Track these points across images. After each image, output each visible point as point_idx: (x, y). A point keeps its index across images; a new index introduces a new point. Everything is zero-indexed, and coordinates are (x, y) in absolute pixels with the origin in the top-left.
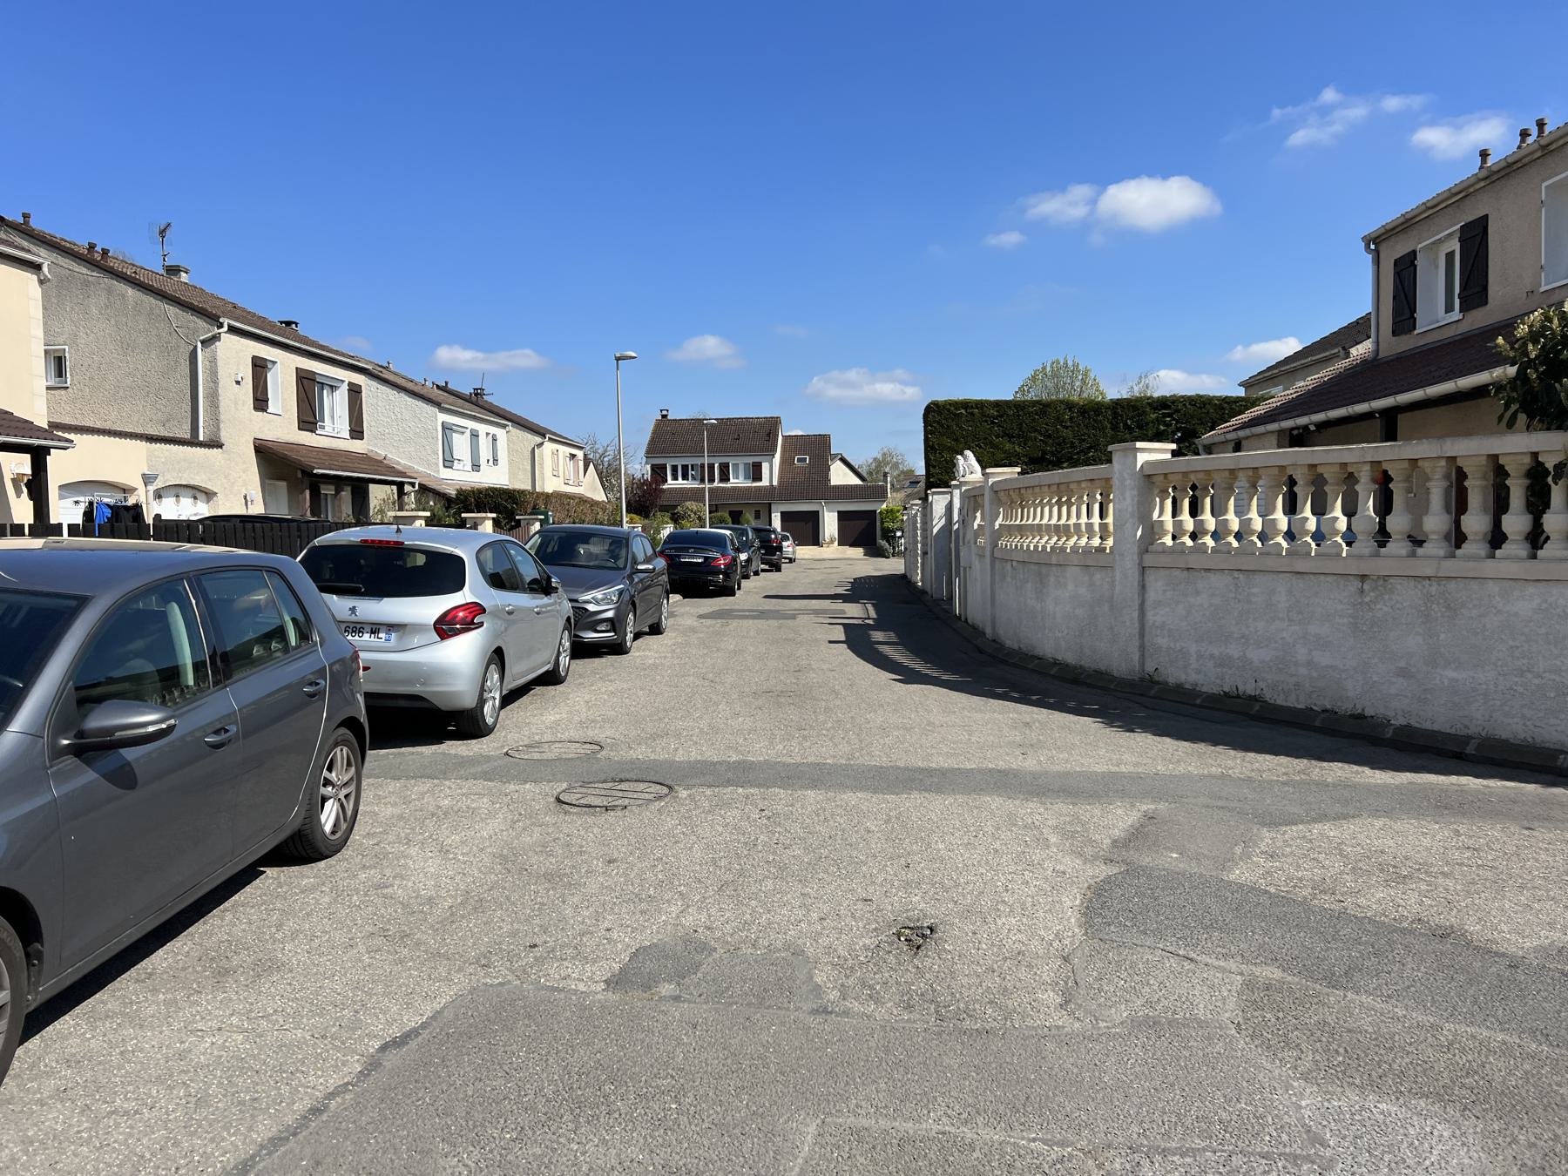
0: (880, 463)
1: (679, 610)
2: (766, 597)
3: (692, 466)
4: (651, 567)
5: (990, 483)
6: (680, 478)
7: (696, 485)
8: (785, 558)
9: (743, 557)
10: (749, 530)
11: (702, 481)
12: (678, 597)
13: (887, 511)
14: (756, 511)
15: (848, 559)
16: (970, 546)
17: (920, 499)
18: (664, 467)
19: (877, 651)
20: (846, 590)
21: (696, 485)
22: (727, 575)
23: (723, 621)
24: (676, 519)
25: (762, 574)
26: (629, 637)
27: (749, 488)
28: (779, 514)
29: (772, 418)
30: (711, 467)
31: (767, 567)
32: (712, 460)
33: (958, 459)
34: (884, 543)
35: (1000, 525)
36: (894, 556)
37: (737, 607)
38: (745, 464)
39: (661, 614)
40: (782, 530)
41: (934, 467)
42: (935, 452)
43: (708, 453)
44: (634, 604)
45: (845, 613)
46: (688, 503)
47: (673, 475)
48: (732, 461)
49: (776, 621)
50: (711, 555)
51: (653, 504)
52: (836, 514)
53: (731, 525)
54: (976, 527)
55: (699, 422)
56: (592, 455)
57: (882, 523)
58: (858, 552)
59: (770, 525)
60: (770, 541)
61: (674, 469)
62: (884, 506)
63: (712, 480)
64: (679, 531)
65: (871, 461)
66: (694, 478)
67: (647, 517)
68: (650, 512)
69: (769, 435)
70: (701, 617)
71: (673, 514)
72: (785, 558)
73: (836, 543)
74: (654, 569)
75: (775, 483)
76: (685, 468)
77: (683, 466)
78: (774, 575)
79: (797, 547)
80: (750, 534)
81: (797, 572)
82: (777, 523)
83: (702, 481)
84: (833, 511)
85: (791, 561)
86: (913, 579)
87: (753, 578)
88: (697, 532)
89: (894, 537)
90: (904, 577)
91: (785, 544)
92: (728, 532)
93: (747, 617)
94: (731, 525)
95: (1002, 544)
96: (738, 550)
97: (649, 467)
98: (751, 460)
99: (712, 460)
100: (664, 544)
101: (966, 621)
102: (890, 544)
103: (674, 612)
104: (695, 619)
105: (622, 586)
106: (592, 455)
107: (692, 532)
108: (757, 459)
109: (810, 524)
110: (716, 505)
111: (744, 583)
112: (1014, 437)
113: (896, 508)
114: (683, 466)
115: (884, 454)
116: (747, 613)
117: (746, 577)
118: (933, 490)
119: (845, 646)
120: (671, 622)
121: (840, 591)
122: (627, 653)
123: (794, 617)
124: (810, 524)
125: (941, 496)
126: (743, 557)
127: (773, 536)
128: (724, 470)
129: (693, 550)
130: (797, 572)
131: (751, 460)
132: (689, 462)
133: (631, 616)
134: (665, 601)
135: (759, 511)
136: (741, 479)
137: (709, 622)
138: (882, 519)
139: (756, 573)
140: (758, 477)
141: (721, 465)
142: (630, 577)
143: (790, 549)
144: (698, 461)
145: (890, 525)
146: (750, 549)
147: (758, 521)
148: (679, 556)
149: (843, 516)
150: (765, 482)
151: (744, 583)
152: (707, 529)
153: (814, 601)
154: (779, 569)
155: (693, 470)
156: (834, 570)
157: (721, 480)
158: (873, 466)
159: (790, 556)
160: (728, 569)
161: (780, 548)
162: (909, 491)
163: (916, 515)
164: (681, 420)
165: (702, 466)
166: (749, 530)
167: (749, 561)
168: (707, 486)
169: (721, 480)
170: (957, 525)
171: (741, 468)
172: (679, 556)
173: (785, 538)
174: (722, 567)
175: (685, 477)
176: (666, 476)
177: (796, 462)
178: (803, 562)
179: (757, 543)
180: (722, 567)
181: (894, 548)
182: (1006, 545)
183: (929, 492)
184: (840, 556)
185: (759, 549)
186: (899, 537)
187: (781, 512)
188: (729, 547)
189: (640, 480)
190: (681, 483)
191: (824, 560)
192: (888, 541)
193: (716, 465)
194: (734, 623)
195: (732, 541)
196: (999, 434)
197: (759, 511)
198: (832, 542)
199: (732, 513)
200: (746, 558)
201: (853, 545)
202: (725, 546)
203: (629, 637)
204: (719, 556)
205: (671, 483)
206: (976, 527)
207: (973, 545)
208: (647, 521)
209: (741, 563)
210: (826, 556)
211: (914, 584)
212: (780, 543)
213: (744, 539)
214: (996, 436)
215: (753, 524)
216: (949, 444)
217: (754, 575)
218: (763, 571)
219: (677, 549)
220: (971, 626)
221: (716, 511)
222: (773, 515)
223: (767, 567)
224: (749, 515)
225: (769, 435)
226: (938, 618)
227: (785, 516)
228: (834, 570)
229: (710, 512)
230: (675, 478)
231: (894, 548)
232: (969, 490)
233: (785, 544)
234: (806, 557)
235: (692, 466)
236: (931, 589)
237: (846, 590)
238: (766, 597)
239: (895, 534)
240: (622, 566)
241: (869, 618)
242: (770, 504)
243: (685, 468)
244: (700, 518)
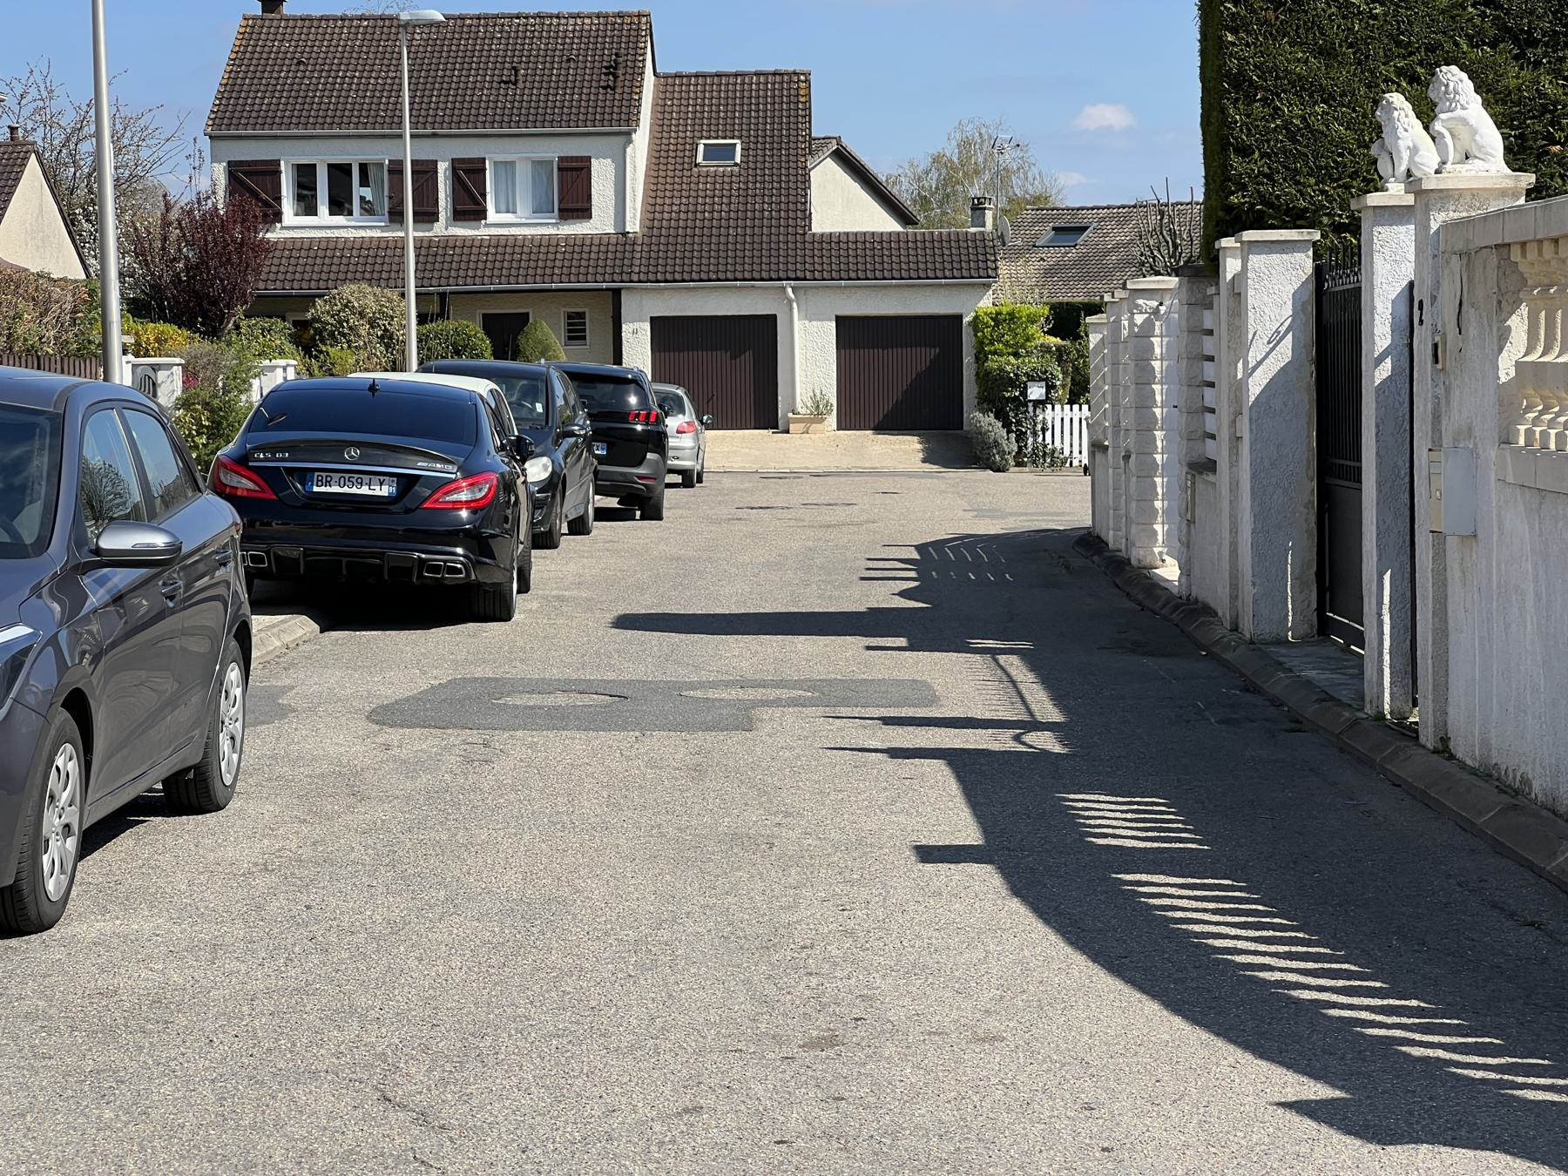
0: (951, 174)
1: (306, 684)
2: (626, 622)
3: (363, 168)
4: (159, 540)
5: (1434, 226)
6: (323, 208)
7: (371, 230)
8: (671, 471)
9: (537, 470)
10: (555, 376)
11: (396, 216)
12: (301, 626)
13: (997, 319)
14: (570, 316)
15: (875, 473)
16: (1473, 453)
17: (1176, 272)
18: (270, 171)
19: (1131, 900)
20: (903, 594)
21: (371, 230)
22: (480, 544)
23: (474, 736)
24: (308, 340)
25: (600, 529)
26: (59, 848)
27: (549, 244)
28: (647, 326)
29: (620, 15)
30: (425, 172)
31: (612, 502)
32: (427, 151)
33: (1391, 108)
34: (988, 423)
35: (1518, 364)
36: (1019, 464)
37: (518, 671)
38: (539, 164)
39: (216, 725)
40: (658, 376)
41: (1244, 152)
42: (1251, 100)
43: (414, 125)
44: (78, 704)
45: (934, 700)
46: (348, 290)
47: (300, 198)
48: (492, 153)
49: (674, 738)
50: (421, 468)
51: (234, 294)
52: (832, 326)
53: (489, 361)
54: (1506, 369)
55: (388, 25)
56: (40, 132)
57: (981, 357)
58: (905, 450)
59: (618, 359)
60: (624, 416)
61: (306, 176)
62: (986, 303)
63: (426, 215)
64: (322, 380)
65: (925, 163)
66: (368, 209)
67: (213, 331)
68: (222, 319)
69: (612, 70)
70: (386, 715)
71: (302, 325)
72: (671, 471)
73: (832, 420)
74: (174, 549)
75: (634, 225)
76: (340, 173)
77: (332, 168)
78: (635, 531)
79: (710, 433)
80: (559, 389)
81: (718, 521)
82: (638, 353)
83: (396, 216)
84: (821, 318)
85: (689, 479)
86: (1136, 555)
87: (568, 543)
88: (373, 387)
89: (1021, 403)
90: (1088, 541)
91: (672, 423)
92: (482, 387)
93: (557, 719)
94: (489, 361)
95: (1529, 433)
96: (520, 451)
97: (220, 172)
98: (554, 150)
99: (427, 151)
100: (249, 429)
101: (1444, 749)
102: (1007, 425)
103: (284, 690)
104: (363, 726)
105: (21, 631)
106: (40, 132)
107: (354, 388)
108: (574, 148)
109: (748, 356)
110: (442, 295)
111: (542, 562)
112: (1534, 43)
113: (1026, 310)
114: (332, 168)
115: (966, 144)
116: (561, 699)
117: (545, 540)
118: (1250, 235)
119: (985, 879)
120: (260, 742)
121: (885, 596)
122: (42, 925)
123: (741, 718)
124: (748, 356)
125: (1276, 258)
126: (537, 470)
127: (633, 400)
128: (469, 177)
129: (355, 452)
130: (718, 521)
131: (554, 150)
132: (352, 153)
133: (66, 761)
134: (234, 674)
135: (581, 315)
136: (523, 212)
137: (414, 742)
138: (981, 343)
139: (579, 527)
140: (575, 204)
141: (457, 166)
142: (67, 585)
143: (687, 441)
144: (379, 153)
145: (1010, 364)
146: (557, 443)
147: (576, 347)
148: (304, 475)
149: (852, 332)
150: (600, 223)
151: (542, 562)
152: (412, 376)
153: (803, 645)
154: (652, 512)
155: (364, 182)
156: (841, 514)
157: (459, 215)
158: (932, 180)
159: (687, 464)
160: (486, 521)
161: (658, 441)
162: (1053, 256)
163: (1148, 327)
164: (327, 19)
165: (396, 169)
166: (555, 376)
167: (555, 484)
168: (412, 233)
169: (459, 215)
170: (1387, 365)
171: (523, 174)
172: (304, 475)
173: (671, 405)
174: (464, 514)
175: (339, 205)
176: (278, 199)
177: (700, 159)
178: (727, 482)
179: (582, 425)
180: (464, 514)
181: (1021, 437)
182: (1545, 435)
183: (1226, 242)
184: (845, 463)
185: (589, 442)
186: (1037, 403)
187: (653, 320)
188: (491, 440)
189: (190, 213)
190: (324, 223)
191: (795, 475)
192: (1001, 415)
193: (443, 168)
194: (517, 746)
195: (496, 414)
196: (1480, 32)
197: (581, 315)
198: (818, 415)
199: (492, 325)
200: (545, 475)
201: (887, 425)
202: (476, 438)
203: (59, 848)
204: (450, 472)
205: (293, 224)
206: (1506, 369)
207: (1493, 453)
208: (206, 346)
209: (530, 495)
210: (795, 462)
211: (1154, 587)
212: (659, 421)
213: (539, 408)
214: (1470, 38)
215: (563, 358)
216: (1300, 69)
217: (572, 532)
218: (603, 515)
219: (293, 448)
220: (1473, 772)
221: (442, 314)
222: (626, 328)
223: (612, 502)
224: (547, 330)
225: (612, 70)
226: (1297, 724)
227: (666, 332)
228: (841, 514)
229: (422, 319)
230: (307, 205)
231: (1021, 437)
232: (1468, 222)
233: (672, 423)
234: (736, 465)
235: (363, 168)
236: (1234, 597)
237: (903, 594)
238: (626, 622)
239: (1024, 393)
240: (29, 537)
241: (1035, 725)
242: (617, 293)
243: (340, 173)
244: (388, 339)
